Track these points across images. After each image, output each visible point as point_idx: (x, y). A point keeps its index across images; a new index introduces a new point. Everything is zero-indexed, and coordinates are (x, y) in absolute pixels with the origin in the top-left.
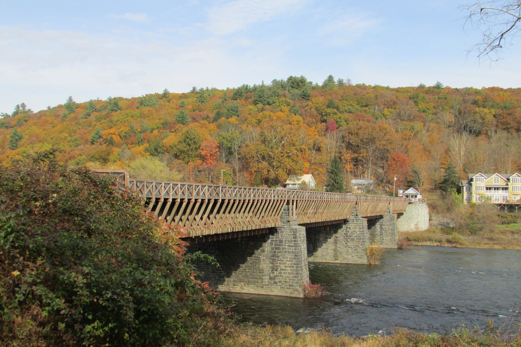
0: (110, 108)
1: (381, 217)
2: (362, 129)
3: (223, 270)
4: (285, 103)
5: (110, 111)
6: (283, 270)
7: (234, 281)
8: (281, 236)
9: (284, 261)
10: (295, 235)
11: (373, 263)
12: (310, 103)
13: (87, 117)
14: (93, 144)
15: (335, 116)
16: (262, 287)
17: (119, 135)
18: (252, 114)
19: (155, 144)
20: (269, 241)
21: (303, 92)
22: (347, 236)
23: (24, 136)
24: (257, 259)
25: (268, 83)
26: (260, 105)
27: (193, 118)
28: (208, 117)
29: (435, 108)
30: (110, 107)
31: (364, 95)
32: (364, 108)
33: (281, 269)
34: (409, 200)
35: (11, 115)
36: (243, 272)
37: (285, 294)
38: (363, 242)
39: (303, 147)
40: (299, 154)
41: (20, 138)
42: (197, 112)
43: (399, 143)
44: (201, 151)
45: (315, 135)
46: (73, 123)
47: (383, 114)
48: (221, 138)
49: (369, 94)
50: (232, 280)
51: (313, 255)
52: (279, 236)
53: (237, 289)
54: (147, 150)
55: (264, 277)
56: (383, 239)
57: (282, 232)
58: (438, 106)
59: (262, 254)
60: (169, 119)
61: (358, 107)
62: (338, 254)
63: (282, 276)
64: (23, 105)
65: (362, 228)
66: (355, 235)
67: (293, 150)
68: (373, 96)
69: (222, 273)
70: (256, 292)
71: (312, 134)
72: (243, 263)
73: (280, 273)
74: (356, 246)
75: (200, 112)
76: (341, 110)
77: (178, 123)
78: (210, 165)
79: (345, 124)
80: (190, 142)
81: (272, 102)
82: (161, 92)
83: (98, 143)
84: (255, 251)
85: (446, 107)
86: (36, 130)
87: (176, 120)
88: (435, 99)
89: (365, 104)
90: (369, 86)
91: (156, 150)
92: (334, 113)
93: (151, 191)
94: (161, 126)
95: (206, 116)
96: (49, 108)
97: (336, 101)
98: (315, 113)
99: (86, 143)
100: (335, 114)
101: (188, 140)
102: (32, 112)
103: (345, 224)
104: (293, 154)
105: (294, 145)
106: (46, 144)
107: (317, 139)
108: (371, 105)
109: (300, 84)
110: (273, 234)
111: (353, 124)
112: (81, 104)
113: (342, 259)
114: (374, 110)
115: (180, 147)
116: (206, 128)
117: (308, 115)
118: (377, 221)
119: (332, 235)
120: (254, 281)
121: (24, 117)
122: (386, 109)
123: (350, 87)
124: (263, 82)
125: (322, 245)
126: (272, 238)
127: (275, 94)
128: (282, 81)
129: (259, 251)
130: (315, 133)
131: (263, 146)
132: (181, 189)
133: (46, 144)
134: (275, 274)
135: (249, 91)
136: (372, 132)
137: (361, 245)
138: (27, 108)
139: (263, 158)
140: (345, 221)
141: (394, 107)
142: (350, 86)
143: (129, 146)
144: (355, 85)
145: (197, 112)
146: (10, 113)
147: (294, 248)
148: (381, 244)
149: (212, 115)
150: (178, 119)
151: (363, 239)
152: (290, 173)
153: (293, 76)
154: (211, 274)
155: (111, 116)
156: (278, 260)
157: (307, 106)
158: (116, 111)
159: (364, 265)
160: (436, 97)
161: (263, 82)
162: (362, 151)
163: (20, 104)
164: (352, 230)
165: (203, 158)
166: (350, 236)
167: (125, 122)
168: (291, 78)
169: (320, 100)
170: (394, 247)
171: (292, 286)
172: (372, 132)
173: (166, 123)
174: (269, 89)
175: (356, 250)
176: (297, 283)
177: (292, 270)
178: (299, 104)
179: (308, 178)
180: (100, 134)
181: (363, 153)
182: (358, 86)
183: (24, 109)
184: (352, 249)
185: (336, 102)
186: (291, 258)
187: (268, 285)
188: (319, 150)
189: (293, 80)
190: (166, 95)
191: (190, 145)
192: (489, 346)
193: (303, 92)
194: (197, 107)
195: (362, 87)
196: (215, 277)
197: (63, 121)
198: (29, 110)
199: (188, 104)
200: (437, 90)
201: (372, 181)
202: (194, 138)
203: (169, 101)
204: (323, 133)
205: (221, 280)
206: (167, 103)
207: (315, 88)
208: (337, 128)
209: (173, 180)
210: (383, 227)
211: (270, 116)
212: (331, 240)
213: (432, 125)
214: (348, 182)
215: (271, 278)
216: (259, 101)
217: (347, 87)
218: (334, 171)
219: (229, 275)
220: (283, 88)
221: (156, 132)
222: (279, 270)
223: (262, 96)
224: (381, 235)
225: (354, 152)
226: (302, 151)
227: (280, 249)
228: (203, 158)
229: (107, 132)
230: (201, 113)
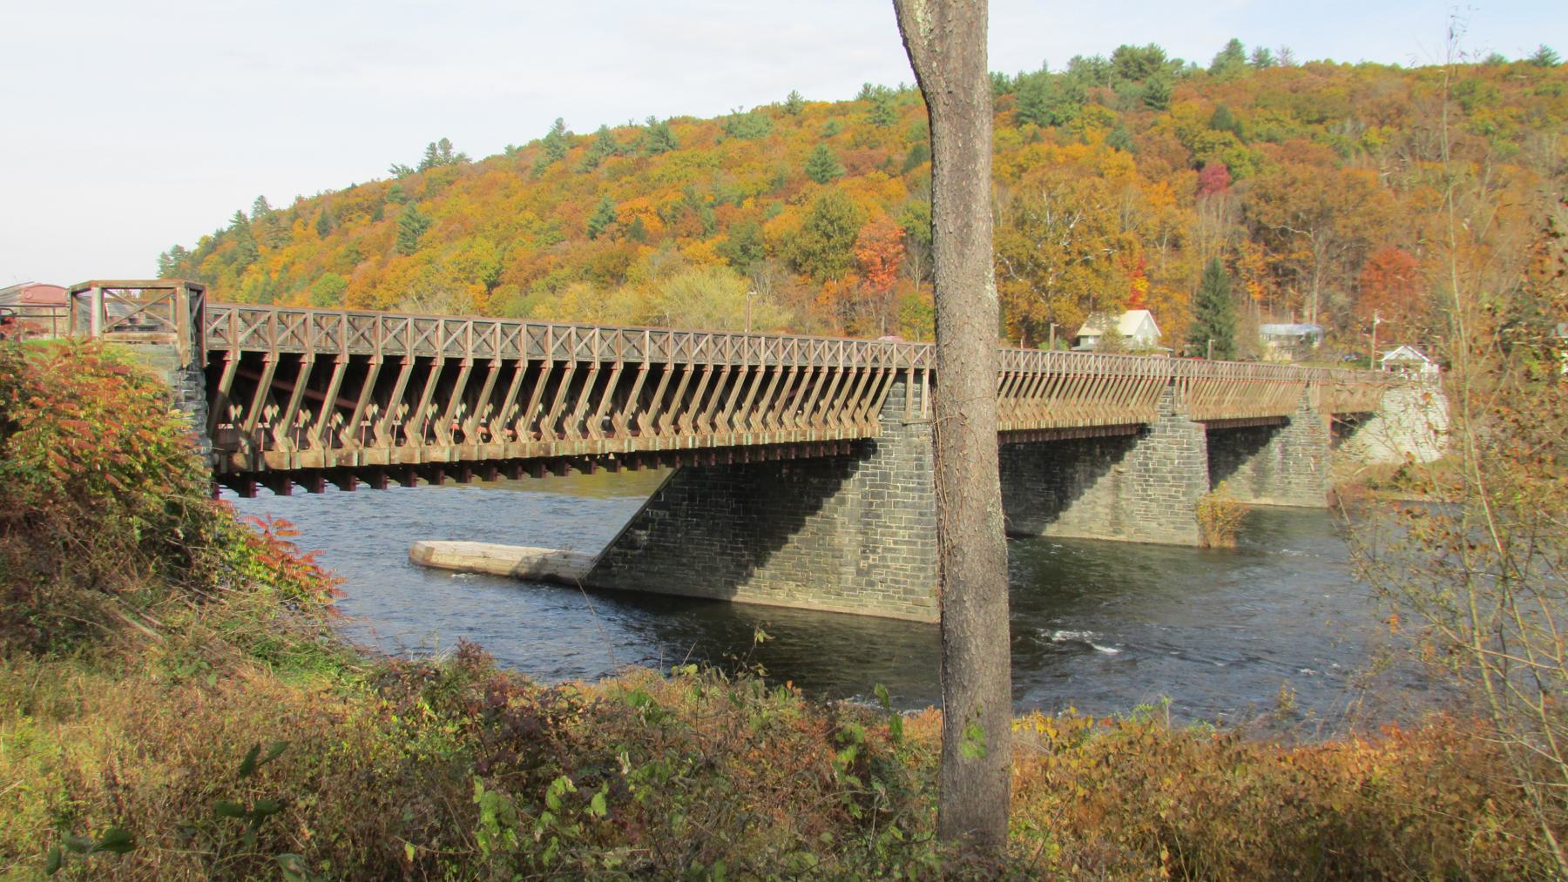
0: (649, 146)
1: (1284, 422)
2: (1299, 184)
3: (746, 549)
4: (1099, 119)
5: (649, 153)
6: (890, 550)
7: (773, 577)
8: (886, 463)
10: (919, 459)
11: (1214, 544)
12: (1164, 118)
13: (589, 168)
14: (593, 237)
15: (1228, 151)
16: (839, 595)
17: (659, 215)
18: (1004, 152)
19: (743, 235)
20: (857, 475)
21: (1151, 88)
22: (1147, 471)
23: (436, 221)
24: (827, 523)
25: (1058, 67)
26: (1030, 127)
27: (852, 165)
28: (889, 161)
29: (1522, 122)
30: (649, 142)
31: (1319, 91)
32: (1311, 128)
33: (885, 549)
34: (1394, 376)
35: (416, 170)
36: (793, 553)
37: (895, 615)
38: (1188, 486)
39: (1129, 235)
40: (1116, 254)
41: (422, 227)
42: (864, 148)
43: (1401, 222)
44: (858, 252)
45: (1168, 204)
46: (553, 186)
47: (1365, 145)
48: (910, 215)
49: (1332, 89)
50: (767, 573)
51: (1057, 518)
53: (780, 598)
54: (721, 251)
55: (844, 569)
57: (889, 453)
58: (1529, 115)
59: (840, 509)
60: (789, 169)
61: (1295, 125)
62: (1123, 517)
63: (888, 567)
64: (445, 144)
65: (1188, 449)
66: (1169, 467)
67: (1099, 245)
68: (1342, 92)
69: (743, 556)
70: (824, 607)
71: (1159, 203)
72: (796, 531)
73: (883, 558)
74: (1170, 496)
75: (871, 148)
76: (1246, 134)
77: (810, 179)
78: (880, 287)
79: (1252, 173)
80: (830, 228)
81: (1062, 117)
82: (783, 100)
83: (604, 236)
84: (825, 500)
85: (1554, 118)
86: (468, 207)
87: (807, 171)
88: (1525, 95)
89: (1316, 117)
90: (1345, 65)
91: (745, 250)
92: (1224, 144)
93: (301, 335)
94: (766, 188)
95: (885, 159)
96: (509, 148)
97: (1239, 109)
98: (1174, 144)
99: (578, 235)
100: (1227, 144)
101: (825, 222)
102: (467, 160)
103: (1141, 438)
104: (1098, 257)
105: (1101, 232)
106: (480, 239)
107: (1171, 216)
108: (1334, 118)
109: (1147, 67)
110: (866, 458)
111: (1273, 173)
112: (586, 136)
113: (1133, 530)
114: (1342, 131)
115: (804, 242)
116: (880, 190)
117: (1154, 149)
118: (1274, 432)
119: (1108, 467)
120: (819, 578)
121: (447, 174)
122: (1373, 129)
123: (1289, 71)
124: (1045, 66)
125: (1082, 493)
126: (865, 468)
127: (1073, 97)
128: (1097, 59)
129: (832, 500)
130: (1167, 199)
131: (1017, 237)
132: (785, 348)
133: (480, 239)
134: (870, 561)
135: (1006, 89)
136: (1324, 192)
137: (1184, 494)
138: (455, 152)
139: (1020, 268)
140: (1142, 430)
141: (1397, 121)
142: (1288, 66)
143: (679, 240)
144: (1301, 64)
145: (864, 148)
146: (414, 166)
147: (916, 495)
148: (1284, 495)
149: (900, 157)
150: (811, 169)
151: (1189, 479)
152: (1091, 304)
153: (1129, 45)
154: (718, 558)
155: (648, 165)
156: (877, 526)
157: (1153, 125)
158: (663, 151)
159: (1190, 547)
160: (1529, 90)
161: (1045, 66)
162: (1296, 244)
163: (437, 142)
164: (1161, 453)
165: (862, 269)
166: (1155, 470)
167: (679, 179)
168: (1121, 52)
169: (1192, 110)
170: (1319, 505)
171: (912, 592)
172: (1324, 192)
173: (781, 179)
174: (1060, 81)
175: (1171, 507)
176: (923, 585)
177: (911, 551)
178: (1136, 121)
179: (1136, 325)
180: (610, 213)
181: (1299, 250)
182: (1311, 68)
183: (447, 154)
184: (1159, 506)
185: (1236, 113)
186: (910, 521)
187: (854, 590)
188: (1175, 245)
189: (1127, 56)
190: (793, 110)
191: (829, 237)
193: (1151, 88)
194: (865, 136)
195: (1322, 70)
196: (727, 567)
197: (534, 180)
198: (461, 156)
199: (846, 130)
200: (1535, 71)
201: (1314, 329)
202: (840, 219)
203: (799, 124)
204: (1190, 198)
205: (740, 574)
206: (794, 129)
207: (1191, 77)
208: (1229, 184)
209: (766, 328)
210: (1290, 449)
211: (1049, 155)
212: (1104, 481)
213: (1508, 170)
214: (1253, 332)
215: (860, 572)
216: (1029, 116)
217: (1276, 70)
218: (1210, 301)
219: (760, 561)
220: (1099, 78)
221: (748, 204)
222: (880, 550)
223: (1037, 101)
224: (1282, 470)
225: (1275, 250)
226: (1122, 248)
227: (883, 498)
228: (862, 269)
229: (627, 206)
230: (873, 152)
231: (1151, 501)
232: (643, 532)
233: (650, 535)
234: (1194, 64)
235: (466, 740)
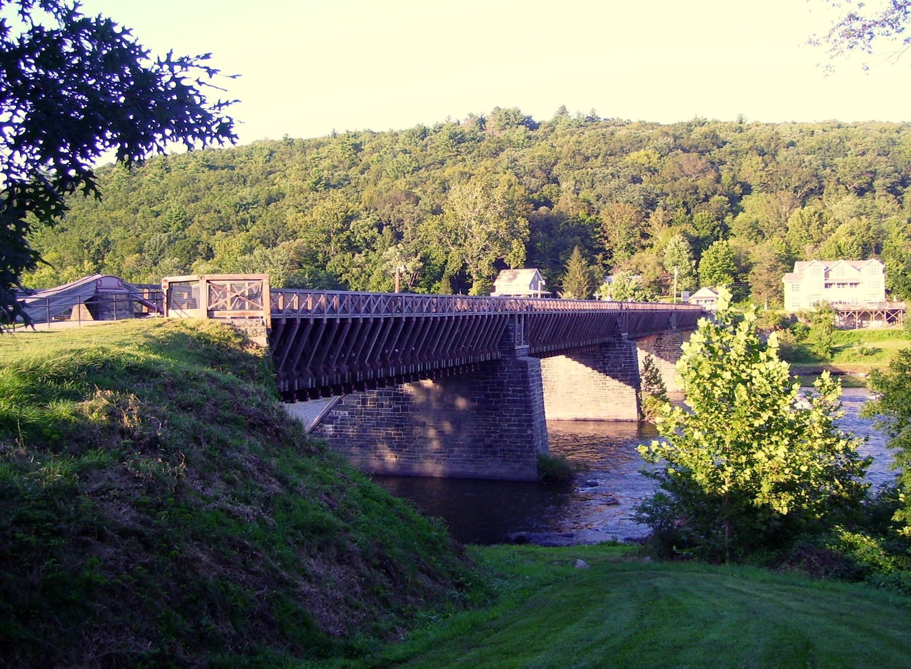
6: (506, 431)
33: (502, 430)
57: (503, 368)
65: (630, 357)
171: (521, 456)
232: (331, 426)
233: (335, 427)
234: (579, 114)
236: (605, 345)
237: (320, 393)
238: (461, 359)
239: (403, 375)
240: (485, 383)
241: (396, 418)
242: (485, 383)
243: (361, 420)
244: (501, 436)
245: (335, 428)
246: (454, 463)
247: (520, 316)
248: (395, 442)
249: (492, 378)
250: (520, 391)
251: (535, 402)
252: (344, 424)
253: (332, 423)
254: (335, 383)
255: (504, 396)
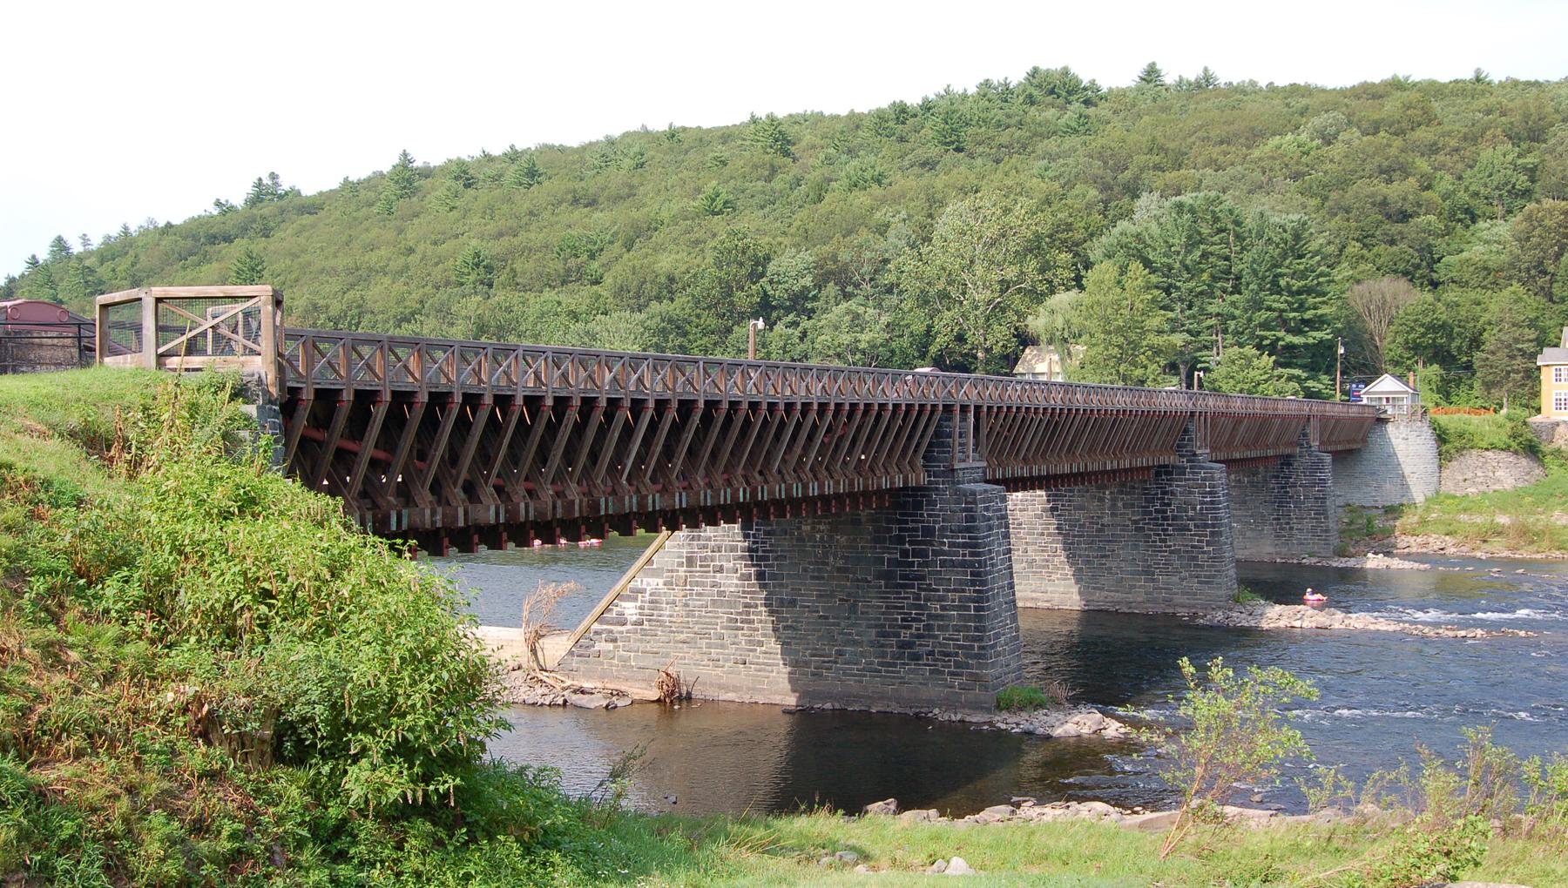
6: (937, 617)
9: (938, 590)
33: (930, 616)
52: (922, 515)
56: (1291, 529)
57: (932, 503)
63: (936, 637)
65: (1210, 493)
74: (1193, 547)
138: (285, 186)
184: (1180, 558)
192: (864, 885)
231: (1172, 552)
232: (633, 604)
235: (114, 797)
236: (1164, 471)
237: (701, 518)
238: (837, 483)
239: (887, 489)
240: (901, 530)
241: (744, 592)
242: (901, 530)
243: (685, 596)
244: (928, 627)
245: (642, 608)
246: (845, 674)
247: (964, 409)
248: (743, 635)
249: (913, 521)
250: (964, 545)
251: (993, 565)
252: (656, 602)
253: (636, 599)
254: (702, 504)
255: (935, 553)
